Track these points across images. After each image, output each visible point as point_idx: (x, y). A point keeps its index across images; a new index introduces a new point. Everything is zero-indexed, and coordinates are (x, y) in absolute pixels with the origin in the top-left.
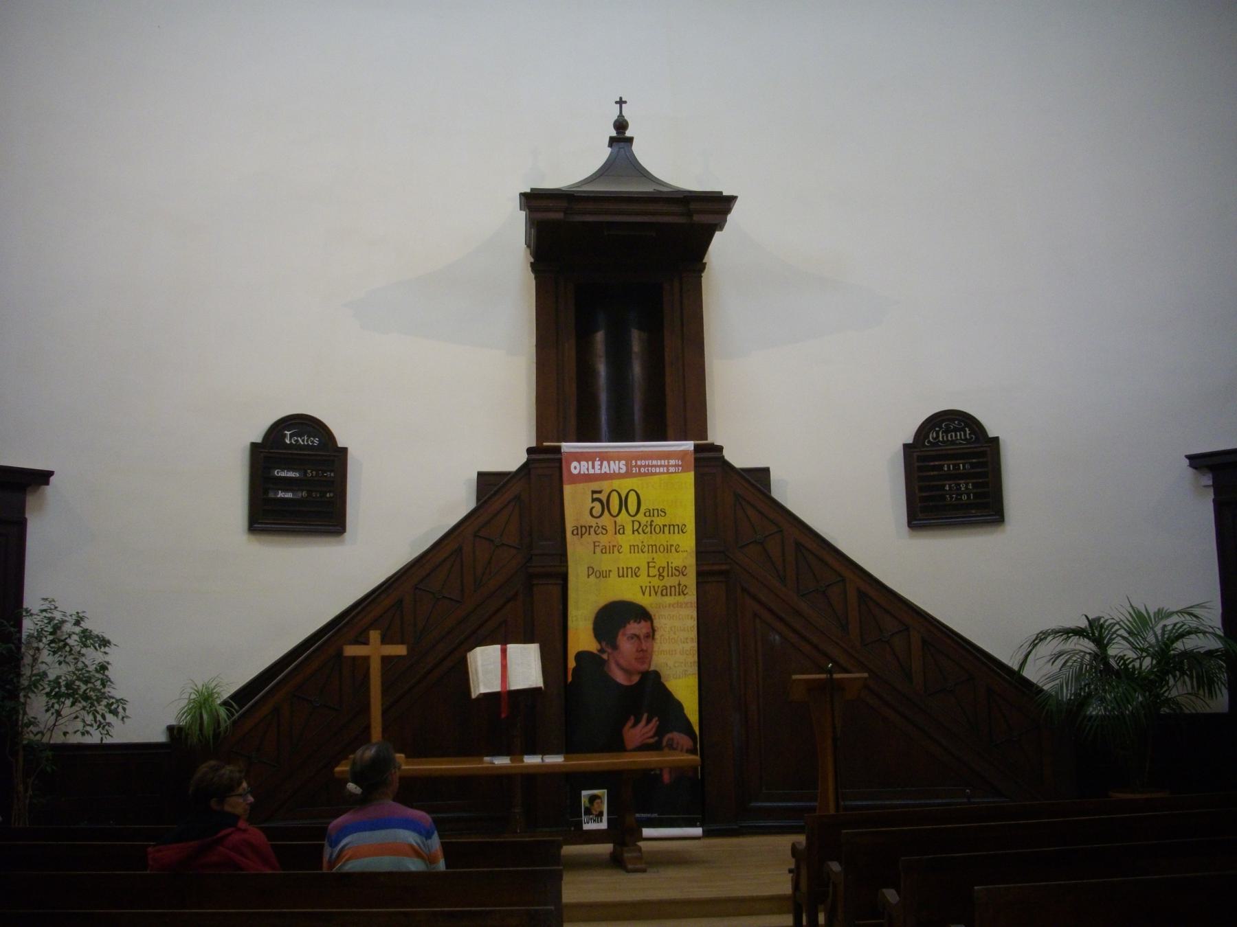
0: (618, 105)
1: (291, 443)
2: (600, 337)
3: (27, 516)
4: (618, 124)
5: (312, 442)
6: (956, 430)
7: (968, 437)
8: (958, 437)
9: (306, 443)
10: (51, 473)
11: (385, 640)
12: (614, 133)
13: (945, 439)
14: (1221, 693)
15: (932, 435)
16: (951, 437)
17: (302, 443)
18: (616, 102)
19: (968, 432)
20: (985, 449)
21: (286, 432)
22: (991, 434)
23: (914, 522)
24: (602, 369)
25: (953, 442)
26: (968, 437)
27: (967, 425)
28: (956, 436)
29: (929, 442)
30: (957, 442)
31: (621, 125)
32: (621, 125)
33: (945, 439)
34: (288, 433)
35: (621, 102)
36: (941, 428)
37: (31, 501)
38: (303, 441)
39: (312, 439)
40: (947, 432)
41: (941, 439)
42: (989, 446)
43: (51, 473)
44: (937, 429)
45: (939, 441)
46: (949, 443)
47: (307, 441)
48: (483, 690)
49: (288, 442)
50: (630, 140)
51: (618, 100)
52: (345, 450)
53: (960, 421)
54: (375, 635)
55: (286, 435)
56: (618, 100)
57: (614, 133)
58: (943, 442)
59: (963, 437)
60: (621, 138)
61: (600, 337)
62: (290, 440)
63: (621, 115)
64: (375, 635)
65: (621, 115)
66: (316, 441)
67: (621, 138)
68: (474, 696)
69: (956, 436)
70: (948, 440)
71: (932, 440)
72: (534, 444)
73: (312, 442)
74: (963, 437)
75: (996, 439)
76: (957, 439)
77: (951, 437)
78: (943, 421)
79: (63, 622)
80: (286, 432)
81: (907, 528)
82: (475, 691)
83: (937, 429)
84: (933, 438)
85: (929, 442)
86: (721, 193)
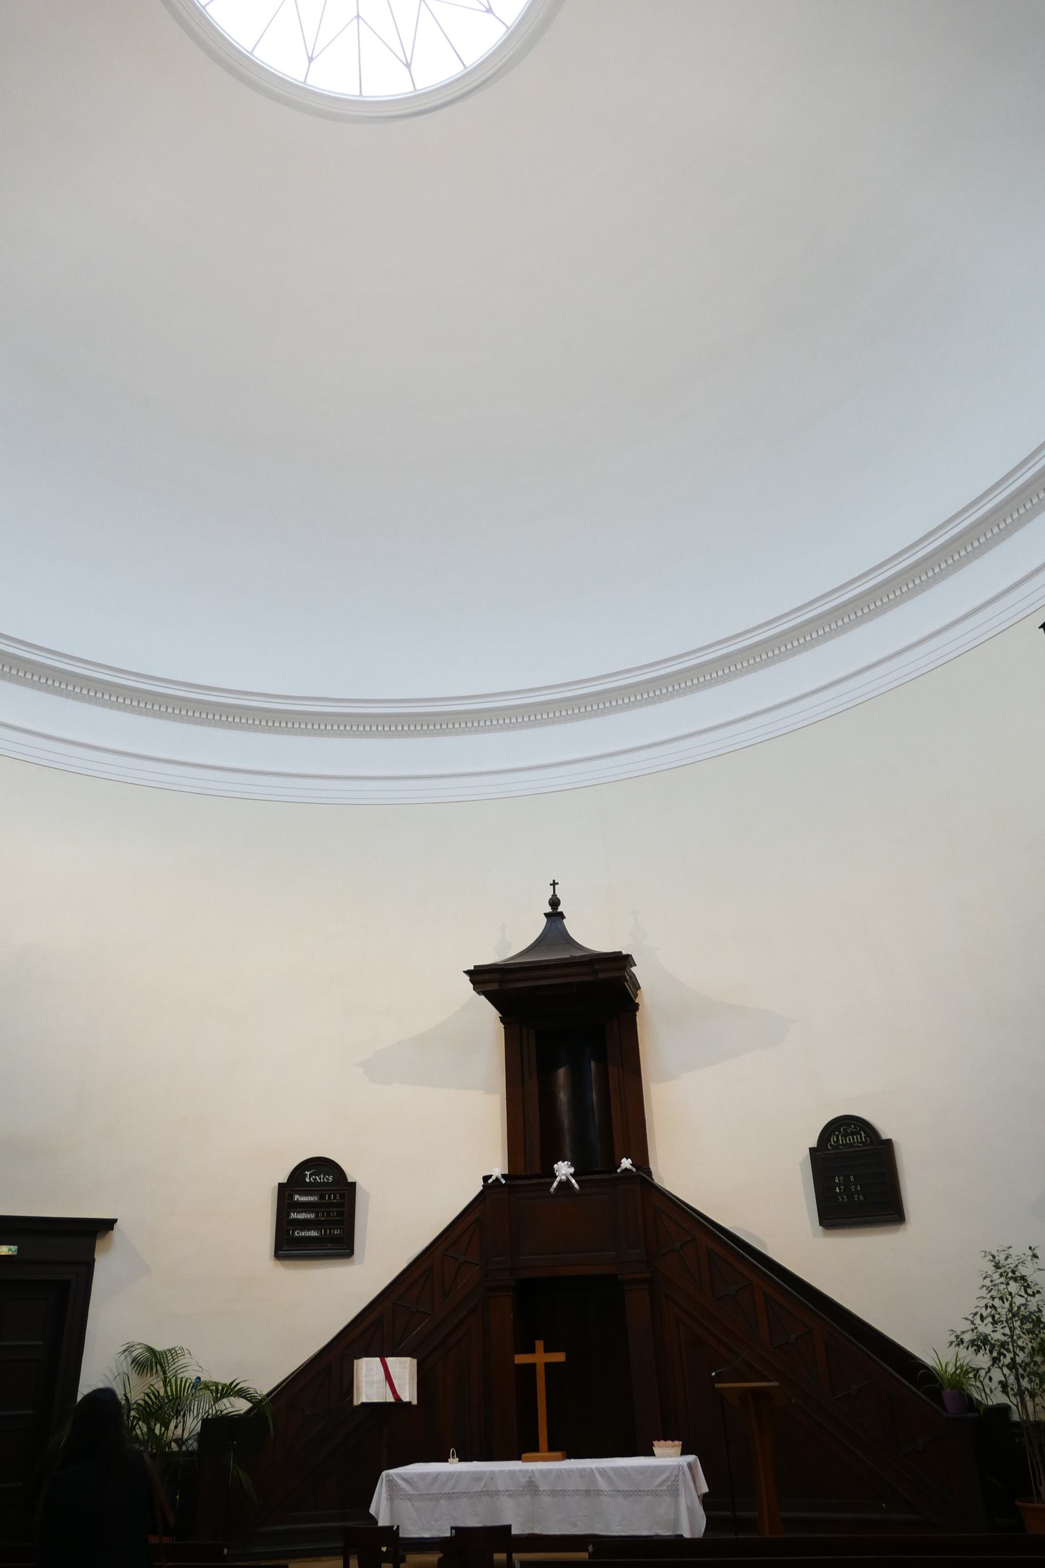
0: (552, 887)
1: (310, 1181)
2: (562, 1074)
3: (96, 1256)
4: (551, 901)
5: (328, 1179)
6: (853, 1134)
7: (864, 1140)
8: (856, 1141)
9: (322, 1181)
10: (115, 1221)
11: (548, 1349)
12: (549, 910)
13: (844, 1142)
14: (235, 1380)
15: (833, 1139)
16: (850, 1140)
17: (319, 1181)
18: (551, 885)
19: (863, 1135)
20: (344, 1192)
21: (306, 1172)
22: (885, 1136)
23: (279, 1252)
24: (563, 1096)
25: (851, 1145)
26: (864, 1140)
27: (861, 1129)
28: (853, 1139)
29: (831, 1145)
30: (855, 1145)
31: (555, 902)
32: (555, 902)
33: (844, 1142)
34: (308, 1173)
35: (554, 884)
36: (840, 1132)
37: (99, 1244)
38: (320, 1179)
39: (327, 1177)
40: (845, 1136)
41: (841, 1142)
42: (347, 1190)
43: (115, 1221)
44: (837, 1133)
45: (840, 1144)
46: (848, 1146)
47: (323, 1179)
48: (364, 1400)
49: (308, 1180)
50: (561, 916)
51: (552, 882)
52: (354, 1184)
53: (855, 1125)
54: (539, 1345)
55: (306, 1175)
56: (552, 882)
57: (549, 910)
58: (843, 1145)
59: (859, 1140)
60: (555, 916)
61: (562, 1074)
62: (310, 1179)
63: (554, 895)
64: (539, 1345)
65: (554, 895)
66: (331, 1179)
67: (555, 916)
68: (356, 1403)
69: (853, 1139)
70: (847, 1143)
71: (833, 1144)
72: (507, 1172)
73: (328, 1179)
74: (859, 1140)
75: (354, 1184)
76: (855, 1142)
77: (850, 1140)
78: (841, 1126)
79: (1030, 1338)
80: (306, 1172)
81: (273, 1257)
82: (357, 1399)
83: (837, 1133)
84: (834, 1141)
85: (831, 1145)
86: (621, 952)
